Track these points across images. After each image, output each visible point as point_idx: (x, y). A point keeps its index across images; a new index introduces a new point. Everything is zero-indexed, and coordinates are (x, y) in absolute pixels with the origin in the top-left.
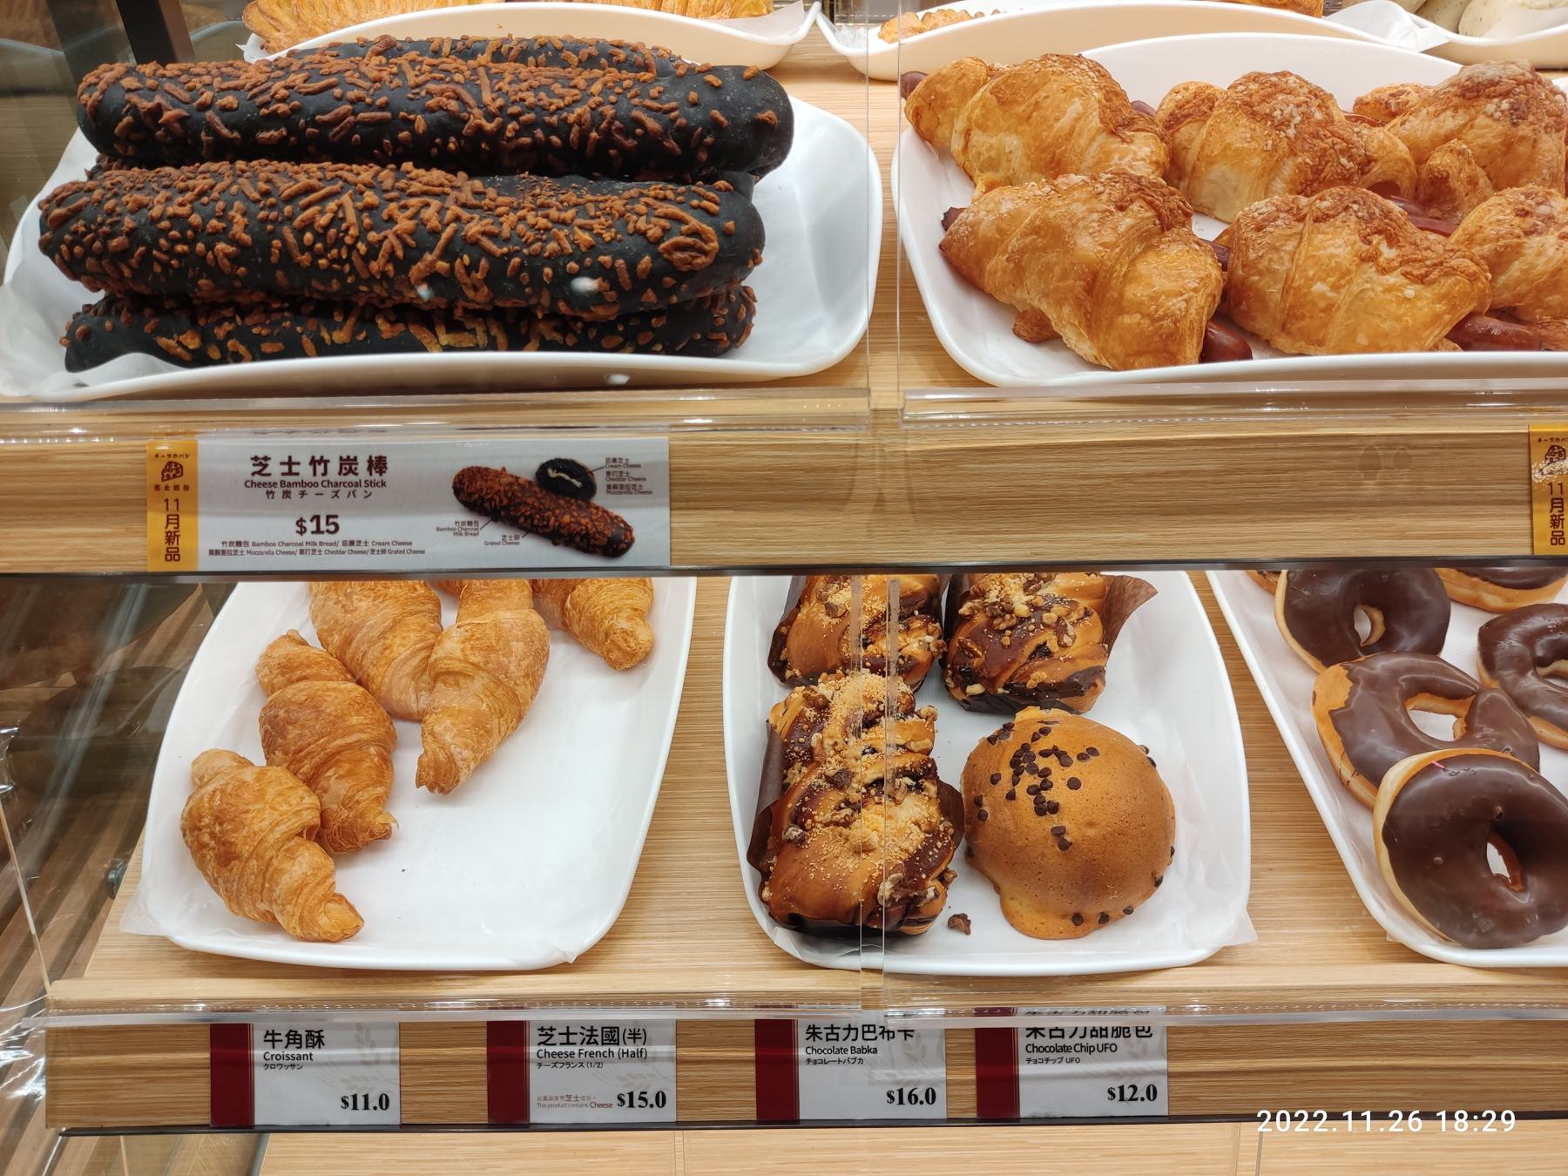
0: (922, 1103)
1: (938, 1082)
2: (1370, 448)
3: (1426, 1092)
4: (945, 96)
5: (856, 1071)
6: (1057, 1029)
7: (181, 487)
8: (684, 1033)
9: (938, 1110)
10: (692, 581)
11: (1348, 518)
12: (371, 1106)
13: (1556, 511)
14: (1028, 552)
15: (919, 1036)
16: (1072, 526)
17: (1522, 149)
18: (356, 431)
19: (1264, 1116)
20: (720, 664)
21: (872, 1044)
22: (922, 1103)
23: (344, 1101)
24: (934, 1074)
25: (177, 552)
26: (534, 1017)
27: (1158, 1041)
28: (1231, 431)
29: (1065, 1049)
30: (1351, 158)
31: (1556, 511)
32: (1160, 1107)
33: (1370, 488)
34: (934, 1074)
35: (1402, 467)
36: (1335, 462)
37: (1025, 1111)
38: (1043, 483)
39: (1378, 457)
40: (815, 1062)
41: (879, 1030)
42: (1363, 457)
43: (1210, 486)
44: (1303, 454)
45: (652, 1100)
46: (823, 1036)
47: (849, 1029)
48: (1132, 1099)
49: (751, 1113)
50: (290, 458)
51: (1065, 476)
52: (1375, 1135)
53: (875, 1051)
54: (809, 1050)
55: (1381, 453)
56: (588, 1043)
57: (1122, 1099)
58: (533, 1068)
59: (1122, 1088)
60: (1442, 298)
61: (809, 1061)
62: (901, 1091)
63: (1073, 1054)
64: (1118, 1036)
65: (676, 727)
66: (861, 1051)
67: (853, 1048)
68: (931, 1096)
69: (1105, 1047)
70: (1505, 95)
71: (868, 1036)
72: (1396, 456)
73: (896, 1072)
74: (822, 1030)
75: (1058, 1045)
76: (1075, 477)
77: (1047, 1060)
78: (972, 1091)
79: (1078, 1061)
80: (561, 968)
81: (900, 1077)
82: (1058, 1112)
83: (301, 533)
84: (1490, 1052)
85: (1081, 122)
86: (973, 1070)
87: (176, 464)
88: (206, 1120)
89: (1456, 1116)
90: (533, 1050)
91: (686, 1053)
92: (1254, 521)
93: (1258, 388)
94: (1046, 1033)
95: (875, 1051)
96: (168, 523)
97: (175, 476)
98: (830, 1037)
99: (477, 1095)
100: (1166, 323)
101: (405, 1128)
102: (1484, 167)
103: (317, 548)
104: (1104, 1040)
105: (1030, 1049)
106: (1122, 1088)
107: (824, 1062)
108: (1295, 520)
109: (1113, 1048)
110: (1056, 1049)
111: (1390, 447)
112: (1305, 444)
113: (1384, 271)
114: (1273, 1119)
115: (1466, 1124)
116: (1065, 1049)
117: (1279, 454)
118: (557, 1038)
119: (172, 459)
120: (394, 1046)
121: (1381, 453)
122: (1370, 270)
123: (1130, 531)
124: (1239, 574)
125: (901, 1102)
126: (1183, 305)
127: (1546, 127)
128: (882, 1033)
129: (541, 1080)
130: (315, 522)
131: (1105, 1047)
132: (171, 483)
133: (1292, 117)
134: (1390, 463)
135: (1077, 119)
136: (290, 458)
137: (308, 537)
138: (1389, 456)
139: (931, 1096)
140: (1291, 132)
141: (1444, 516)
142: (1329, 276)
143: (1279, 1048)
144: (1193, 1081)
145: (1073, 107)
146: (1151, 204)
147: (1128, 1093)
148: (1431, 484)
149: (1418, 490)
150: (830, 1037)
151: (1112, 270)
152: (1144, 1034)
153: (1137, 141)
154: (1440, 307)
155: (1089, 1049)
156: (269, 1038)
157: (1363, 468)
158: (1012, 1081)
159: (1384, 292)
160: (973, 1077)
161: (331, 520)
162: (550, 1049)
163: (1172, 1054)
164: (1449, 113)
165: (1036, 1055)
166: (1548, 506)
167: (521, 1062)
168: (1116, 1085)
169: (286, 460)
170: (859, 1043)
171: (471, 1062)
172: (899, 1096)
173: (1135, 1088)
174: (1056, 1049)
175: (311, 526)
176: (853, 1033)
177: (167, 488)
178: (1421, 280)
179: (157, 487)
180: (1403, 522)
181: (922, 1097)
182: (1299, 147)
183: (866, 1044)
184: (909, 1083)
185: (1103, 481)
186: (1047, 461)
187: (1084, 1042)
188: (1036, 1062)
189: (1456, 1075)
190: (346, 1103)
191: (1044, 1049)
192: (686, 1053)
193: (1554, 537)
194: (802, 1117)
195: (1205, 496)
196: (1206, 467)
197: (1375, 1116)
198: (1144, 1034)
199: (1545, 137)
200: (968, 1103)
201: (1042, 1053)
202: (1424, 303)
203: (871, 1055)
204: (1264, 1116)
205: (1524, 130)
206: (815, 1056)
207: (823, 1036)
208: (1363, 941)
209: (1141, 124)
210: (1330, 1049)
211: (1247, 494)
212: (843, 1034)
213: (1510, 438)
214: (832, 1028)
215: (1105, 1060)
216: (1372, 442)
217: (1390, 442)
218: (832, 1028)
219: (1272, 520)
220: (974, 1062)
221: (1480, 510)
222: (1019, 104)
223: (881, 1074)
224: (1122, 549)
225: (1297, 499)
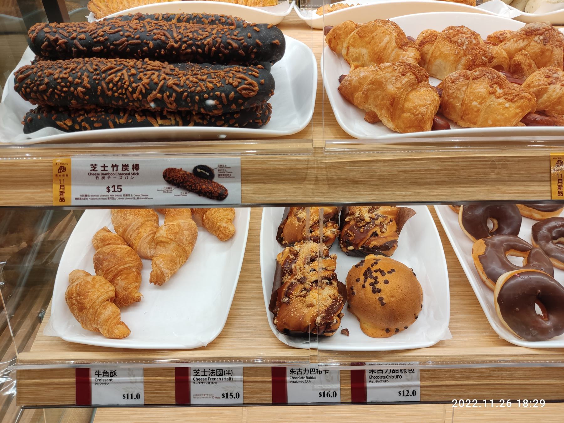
0: (331, 397)
1: (337, 389)
2: (493, 161)
3: (513, 393)
4: (340, 34)
5: (308, 385)
6: (380, 370)
7: (65, 175)
8: (246, 372)
9: (338, 399)
10: (249, 209)
11: (485, 186)
12: (133, 398)
13: (560, 184)
14: (370, 199)
15: (331, 373)
16: (386, 189)
17: (548, 54)
18: (128, 155)
19: (455, 401)
20: (259, 239)
21: (313, 376)
22: (331, 397)
23: (124, 396)
24: (336, 386)
25: (64, 199)
26: (192, 366)
27: (416, 374)
28: (443, 155)
29: (383, 377)
30: (486, 57)
31: (560, 184)
32: (417, 398)
33: (493, 176)
34: (336, 386)
35: (504, 168)
36: (480, 166)
37: (369, 400)
38: (375, 174)
39: (496, 164)
40: (293, 382)
41: (316, 371)
42: (490, 164)
43: (435, 175)
44: (469, 163)
45: (234, 396)
46: (296, 373)
47: (306, 370)
48: (407, 395)
49: (270, 400)
50: (104, 165)
51: (383, 171)
52: (495, 408)
53: (315, 378)
54: (291, 378)
55: (497, 163)
56: (212, 375)
57: (404, 395)
58: (192, 384)
59: (403, 391)
60: (519, 107)
61: (291, 381)
62: (324, 393)
63: (386, 379)
64: (402, 373)
65: (243, 262)
66: (310, 378)
67: (307, 377)
68: (335, 394)
69: (397, 377)
70: (541, 34)
71: (312, 373)
72: (502, 164)
73: (322, 386)
74: (296, 370)
75: (381, 376)
76: (387, 171)
77: (377, 381)
78: (350, 392)
79: (388, 381)
80: (202, 348)
81: (324, 387)
82: (380, 400)
83: (108, 192)
84: (536, 378)
85: (389, 44)
86: (350, 385)
87: (63, 167)
88: (74, 403)
89: (524, 401)
90: (192, 378)
91: (247, 379)
92: (451, 188)
93: (453, 140)
94: (376, 371)
95: (315, 378)
96: (60, 188)
97: (63, 171)
98: (299, 373)
99: (172, 394)
100: (419, 116)
101: (146, 406)
102: (534, 60)
103: (114, 197)
104: (397, 374)
105: (371, 377)
106: (403, 391)
107: (296, 382)
108: (466, 187)
109: (400, 377)
110: (380, 377)
111: (500, 161)
112: (469, 160)
113: (498, 97)
114: (458, 402)
115: (527, 404)
116: (383, 377)
117: (460, 163)
118: (200, 373)
119: (62, 165)
120: (142, 376)
121: (497, 163)
122: (493, 97)
123: (407, 191)
124: (446, 206)
125: (324, 396)
126: (426, 110)
127: (556, 46)
128: (317, 372)
129: (195, 389)
130: (113, 188)
131: (397, 377)
132: (62, 174)
133: (465, 42)
134: (500, 166)
135: (388, 43)
136: (104, 165)
137: (111, 193)
138: (500, 164)
139: (335, 394)
140: (464, 47)
141: (519, 186)
142: (478, 99)
143: (460, 377)
144: (429, 389)
145: (386, 39)
146: (414, 73)
147: (406, 393)
148: (515, 174)
149: (510, 176)
150: (299, 373)
151: (400, 97)
152: (411, 372)
153: (409, 51)
154: (518, 111)
155: (392, 377)
156: (97, 373)
157: (490, 168)
158: (364, 389)
159: (498, 105)
160: (350, 387)
161: (119, 187)
162: (198, 377)
163: (422, 379)
164: (521, 41)
165: (373, 380)
166: (557, 182)
167: (187, 382)
168: (401, 390)
169: (103, 165)
170: (309, 375)
171: (169, 382)
172: (324, 394)
173: (408, 391)
174: (380, 377)
175: (112, 189)
176: (307, 371)
177: (60, 175)
178: (511, 101)
179: (57, 175)
180: (505, 188)
181: (332, 395)
182: (467, 53)
183: (311, 376)
184: (327, 390)
185: (397, 173)
186: (377, 166)
187: (390, 375)
188: (373, 382)
189: (524, 387)
190: (125, 397)
191: (376, 377)
192: (247, 379)
193: (559, 193)
194: (288, 402)
195: (433, 178)
196: (434, 168)
197: (494, 402)
198: (411, 372)
199: (556, 49)
200: (348, 397)
201: (375, 379)
202: (512, 109)
203: (313, 379)
204: (455, 401)
205: (548, 47)
206: (293, 380)
207: (296, 373)
208: (490, 339)
209: (410, 45)
210: (478, 377)
211: (449, 178)
212: (303, 372)
213: (543, 157)
214: (299, 370)
215: (397, 381)
216: (493, 159)
217: (500, 159)
218: (299, 370)
219: (457, 187)
220: (350, 382)
221: (532, 183)
222: (367, 37)
223: (317, 386)
224: (403, 198)
225: (466, 180)
